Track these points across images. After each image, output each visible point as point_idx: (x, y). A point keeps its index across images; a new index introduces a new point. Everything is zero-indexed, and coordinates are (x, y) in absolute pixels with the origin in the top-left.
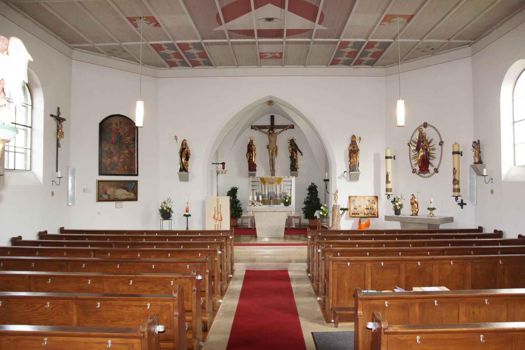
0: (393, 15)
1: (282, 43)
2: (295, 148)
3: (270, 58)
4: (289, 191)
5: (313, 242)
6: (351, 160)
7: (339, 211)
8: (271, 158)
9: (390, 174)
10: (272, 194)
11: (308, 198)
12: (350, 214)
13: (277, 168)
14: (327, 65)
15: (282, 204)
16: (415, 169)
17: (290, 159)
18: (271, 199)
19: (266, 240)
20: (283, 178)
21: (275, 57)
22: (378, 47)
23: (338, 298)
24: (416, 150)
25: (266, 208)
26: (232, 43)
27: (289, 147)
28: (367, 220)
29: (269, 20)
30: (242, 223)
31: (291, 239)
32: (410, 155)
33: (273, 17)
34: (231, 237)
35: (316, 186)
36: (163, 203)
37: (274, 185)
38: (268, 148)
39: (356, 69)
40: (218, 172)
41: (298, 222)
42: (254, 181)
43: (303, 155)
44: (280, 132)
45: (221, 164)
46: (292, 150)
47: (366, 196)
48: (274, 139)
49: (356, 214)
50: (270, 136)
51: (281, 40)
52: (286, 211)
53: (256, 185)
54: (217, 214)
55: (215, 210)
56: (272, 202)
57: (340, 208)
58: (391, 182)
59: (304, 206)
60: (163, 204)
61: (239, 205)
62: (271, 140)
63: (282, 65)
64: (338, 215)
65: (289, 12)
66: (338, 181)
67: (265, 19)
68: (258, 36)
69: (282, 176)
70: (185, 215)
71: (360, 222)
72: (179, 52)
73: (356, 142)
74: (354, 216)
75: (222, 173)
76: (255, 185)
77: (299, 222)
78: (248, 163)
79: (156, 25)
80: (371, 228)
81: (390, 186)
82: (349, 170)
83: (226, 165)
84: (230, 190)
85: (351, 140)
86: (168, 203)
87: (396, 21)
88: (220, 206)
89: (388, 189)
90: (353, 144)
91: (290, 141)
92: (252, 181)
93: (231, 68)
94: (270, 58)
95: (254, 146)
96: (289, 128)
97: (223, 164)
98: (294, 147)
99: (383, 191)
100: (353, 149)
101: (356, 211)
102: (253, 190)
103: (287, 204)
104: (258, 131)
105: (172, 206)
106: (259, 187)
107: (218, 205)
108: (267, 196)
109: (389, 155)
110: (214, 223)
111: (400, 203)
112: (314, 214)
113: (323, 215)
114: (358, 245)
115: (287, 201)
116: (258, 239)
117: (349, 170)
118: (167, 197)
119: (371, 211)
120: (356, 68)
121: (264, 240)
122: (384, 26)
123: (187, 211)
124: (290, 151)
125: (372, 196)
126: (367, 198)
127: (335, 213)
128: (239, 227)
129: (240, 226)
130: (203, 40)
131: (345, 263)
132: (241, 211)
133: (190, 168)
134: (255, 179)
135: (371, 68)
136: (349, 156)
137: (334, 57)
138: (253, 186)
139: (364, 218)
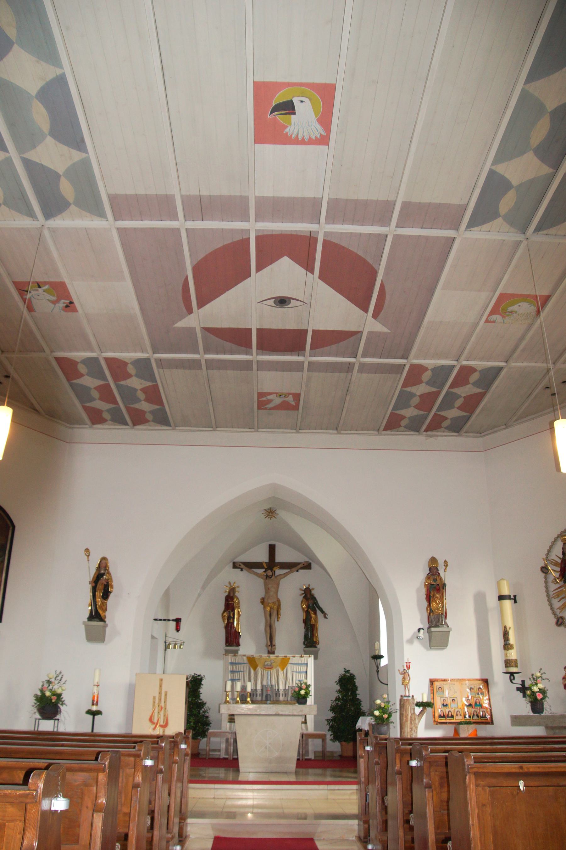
0: (513, 296)
1: (298, 367)
2: (313, 605)
3: (276, 408)
7: (414, 709)
8: (269, 622)
9: (511, 630)
10: (269, 689)
11: (337, 699)
13: (279, 640)
14: (378, 431)
16: (562, 618)
20: (292, 658)
21: (284, 406)
22: (476, 384)
24: (561, 577)
26: (210, 364)
27: (302, 602)
29: (282, 302)
32: (547, 592)
33: (289, 296)
35: (354, 676)
36: (45, 682)
37: (274, 671)
38: (262, 604)
40: (167, 644)
42: (236, 664)
43: (327, 618)
44: (285, 574)
45: (173, 620)
46: (308, 607)
47: (464, 680)
49: (448, 716)
50: (267, 581)
51: (301, 359)
52: (300, 713)
53: (239, 671)
54: (159, 713)
55: (154, 703)
57: (415, 702)
58: (514, 646)
59: (331, 715)
60: (46, 685)
61: (204, 712)
62: (269, 589)
63: (296, 429)
65: (321, 283)
66: (406, 647)
67: (274, 300)
68: (257, 349)
69: (288, 654)
70: (89, 712)
73: (439, 572)
74: (443, 720)
76: (236, 672)
79: (67, 306)
81: (513, 654)
82: (428, 627)
85: (429, 566)
86: (57, 682)
87: (516, 312)
88: (166, 695)
89: (509, 660)
90: (432, 575)
91: (303, 592)
93: (203, 430)
94: (276, 408)
95: (238, 598)
96: (302, 568)
97: (178, 621)
98: (311, 602)
99: (498, 667)
100: (434, 583)
105: (63, 690)
106: (245, 674)
107: (160, 693)
108: (259, 692)
109: (506, 592)
111: (540, 686)
112: (356, 724)
115: (303, 692)
116: (240, 773)
118: (56, 671)
120: (431, 436)
122: (493, 324)
124: (303, 609)
125: (477, 680)
126: (467, 682)
127: (406, 713)
130: (154, 353)
131: (511, 782)
133: (109, 615)
134: (238, 659)
135: (457, 436)
137: (393, 409)
138: (233, 672)
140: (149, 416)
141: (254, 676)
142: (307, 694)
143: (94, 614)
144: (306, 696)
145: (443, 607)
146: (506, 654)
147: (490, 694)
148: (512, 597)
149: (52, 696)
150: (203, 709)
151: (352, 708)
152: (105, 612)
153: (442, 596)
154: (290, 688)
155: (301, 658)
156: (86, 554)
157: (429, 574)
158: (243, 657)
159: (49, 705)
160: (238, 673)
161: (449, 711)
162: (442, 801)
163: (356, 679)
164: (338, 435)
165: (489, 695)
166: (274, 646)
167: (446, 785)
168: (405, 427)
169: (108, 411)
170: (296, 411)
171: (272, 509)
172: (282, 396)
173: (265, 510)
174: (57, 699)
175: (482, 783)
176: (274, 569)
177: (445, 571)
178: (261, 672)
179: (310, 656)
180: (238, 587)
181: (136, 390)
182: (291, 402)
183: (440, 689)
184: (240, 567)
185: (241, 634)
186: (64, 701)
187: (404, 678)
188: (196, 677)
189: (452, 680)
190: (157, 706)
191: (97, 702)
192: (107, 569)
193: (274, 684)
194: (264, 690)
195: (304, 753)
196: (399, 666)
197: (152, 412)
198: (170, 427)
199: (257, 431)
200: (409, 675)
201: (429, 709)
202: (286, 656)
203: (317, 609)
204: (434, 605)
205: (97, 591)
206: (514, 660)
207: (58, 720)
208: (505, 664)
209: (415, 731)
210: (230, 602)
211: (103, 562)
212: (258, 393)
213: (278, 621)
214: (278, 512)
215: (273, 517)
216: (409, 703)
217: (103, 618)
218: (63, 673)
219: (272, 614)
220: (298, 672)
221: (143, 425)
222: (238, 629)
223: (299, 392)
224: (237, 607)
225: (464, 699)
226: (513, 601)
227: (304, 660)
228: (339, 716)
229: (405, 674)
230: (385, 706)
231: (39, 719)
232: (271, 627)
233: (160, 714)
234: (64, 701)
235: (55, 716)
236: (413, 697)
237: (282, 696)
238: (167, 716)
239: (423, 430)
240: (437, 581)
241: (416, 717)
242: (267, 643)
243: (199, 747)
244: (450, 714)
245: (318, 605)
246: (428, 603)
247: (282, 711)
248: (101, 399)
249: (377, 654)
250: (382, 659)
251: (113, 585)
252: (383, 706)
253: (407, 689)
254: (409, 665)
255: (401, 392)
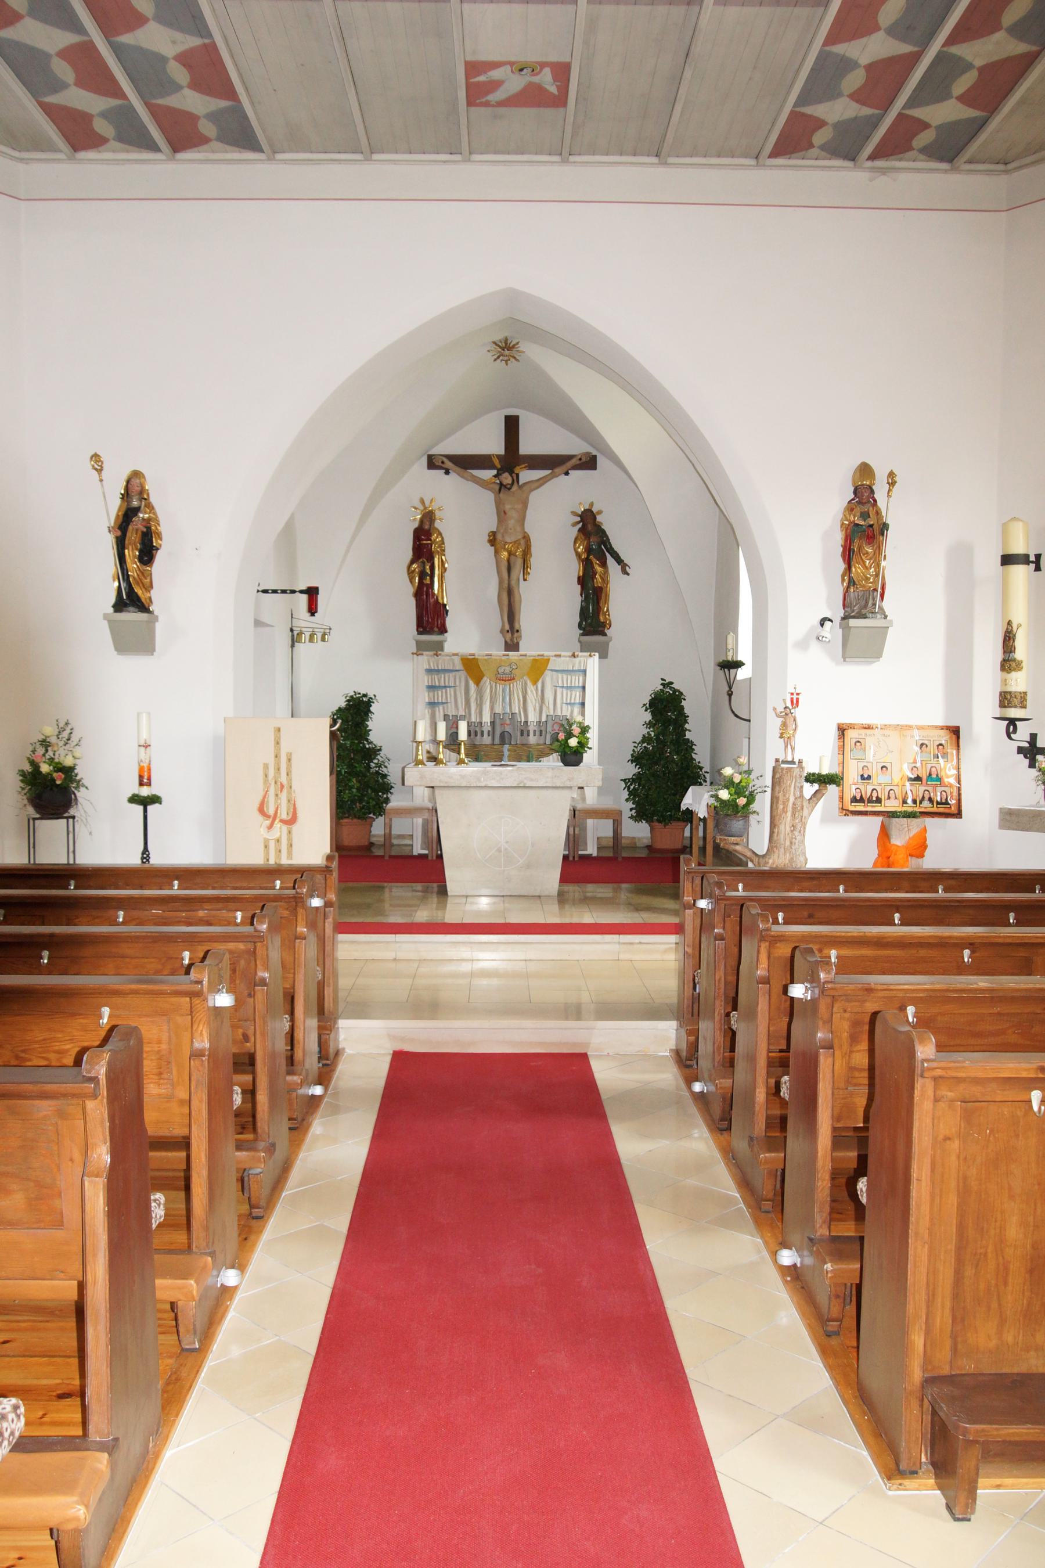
4: (577, 709)
5: (721, 931)
6: (853, 569)
10: (508, 722)
11: (646, 739)
12: (842, 798)
13: (526, 621)
14: (757, 158)
15: (553, 761)
17: (579, 587)
18: (503, 742)
19: (483, 907)
23: (960, 1317)
25: (485, 773)
28: (915, 826)
30: (388, 836)
31: (586, 901)
34: (316, 902)
35: (681, 693)
37: (517, 687)
38: (492, 545)
39: (884, 178)
40: (295, 633)
41: (610, 833)
42: (438, 671)
43: (628, 574)
45: (301, 592)
46: (589, 550)
47: (910, 727)
48: (519, 506)
49: (870, 800)
50: (501, 495)
52: (568, 784)
53: (445, 687)
54: (277, 795)
56: (506, 753)
58: (1024, 665)
59: (632, 770)
60: (41, 751)
61: (379, 766)
62: (505, 513)
64: (799, 803)
70: (134, 799)
71: (884, 834)
72: (91, 42)
74: (860, 807)
75: (311, 640)
76: (440, 687)
77: (611, 834)
78: (412, 602)
80: (931, 862)
81: (1018, 682)
83: (321, 598)
84: (343, 704)
85: (854, 481)
86: (61, 743)
88: (289, 760)
89: (1010, 693)
90: (860, 503)
92: (429, 671)
95: (440, 534)
97: (312, 593)
100: (862, 523)
101: (867, 790)
102: (432, 704)
103: (572, 757)
104: (453, 476)
108: (487, 728)
109: (1018, 548)
110: (263, 831)
113: (734, 800)
114: (973, 952)
115: (573, 742)
116: (450, 900)
117: (841, 613)
119: (930, 789)
120: (883, 171)
121: (474, 907)
123: (144, 780)
124: (578, 555)
125: (936, 727)
126: (916, 732)
128: (379, 852)
129: (380, 846)
131: (1012, 1094)
132: (387, 788)
133: (159, 598)
134: (443, 663)
135: (946, 171)
136: (844, 552)
138: (431, 688)
139: (904, 817)
140: (207, 128)
141: (477, 695)
142: (582, 745)
143: (125, 597)
144: (581, 750)
145: (877, 575)
146: (1006, 680)
147: (961, 757)
148: (1032, 558)
149: (55, 771)
150: (376, 761)
151: (675, 757)
152: (149, 592)
153: (879, 550)
154: (550, 718)
155: (574, 659)
156: (93, 466)
157: (853, 499)
158: (453, 657)
159: (51, 789)
160: (444, 691)
161: (873, 790)
162: (852, 1069)
163: (685, 699)
164: (662, 170)
165: (958, 759)
166: (518, 631)
167: (866, 1037)
168: (822, 148)
169: (104, 115)
170: (561, 110)
171: (509, 342)
172: (525, 70)
173: (494, 343)
174: (65, 779)
175: (949, 1094)
176: (517, 470)
177: (889, 496)
178: (491, 687)
179: (590, 656)
180: (440, 509)
181: (164, 60)
182: (548, 87)
183: (858, 744)
184: (443, 466)
185: (448, 608)
186: (79, 781)
187: (784, 725)
188: (359, 698)
189: (885, 727)
190: (273, 783)
191: (149, 779)
192: (145, 497)
193: (517, 712)
194: (498, 722)
195: (576, 832)
196: (775, 699)
197: (212, 117)
198: (262, 154)
199: (469, 161)
200: (795, 720)
201: (832, 789)
202: (542, 655)
203: (608, 555)
204: (857, 569)
205: (126, 546)
206: (1020, 693)
207: (73, 817)
208: (1000, 701)
209: (800, 832)
210: (425, 542)
211: (136, 481)
212: (467, 63)
213: (525, 580)
214: (522, 347)
215: (512, 360)
216: (792, 776)
217: (147, 606)
218: (73, 724)
219: (512, 565)
220: (567, 688)
221: (196, 149)
222: (443, 598)
223: (568, 60)
224: (438, 552)
225: (905, 767)
226: (1033, 566)
227: (580, 662)
228: (647, 772)
229: (787, 716)
230: (741, 782)
231: (34, 819)
232: (510, 592)
233: (280, 799)
234: (79, 781)
235: (66, 811)
236: (800, 762)
237: (535, 735)
238: (295, 801)
239: (867, 157)
240: (869, 517)
241: (805, 804)
242: (503, 626)
243: (371, 832)
244: (875, 795)
245: (611, 545)
246: (847, 566)
247: (532, 780)
248: (80, 83)
249: (730, 658)
250: (740, 669)
251: (161, 532)
252: (738, 781)
253: (789, 746)
254: (797, 700)
255: (823, 56)
